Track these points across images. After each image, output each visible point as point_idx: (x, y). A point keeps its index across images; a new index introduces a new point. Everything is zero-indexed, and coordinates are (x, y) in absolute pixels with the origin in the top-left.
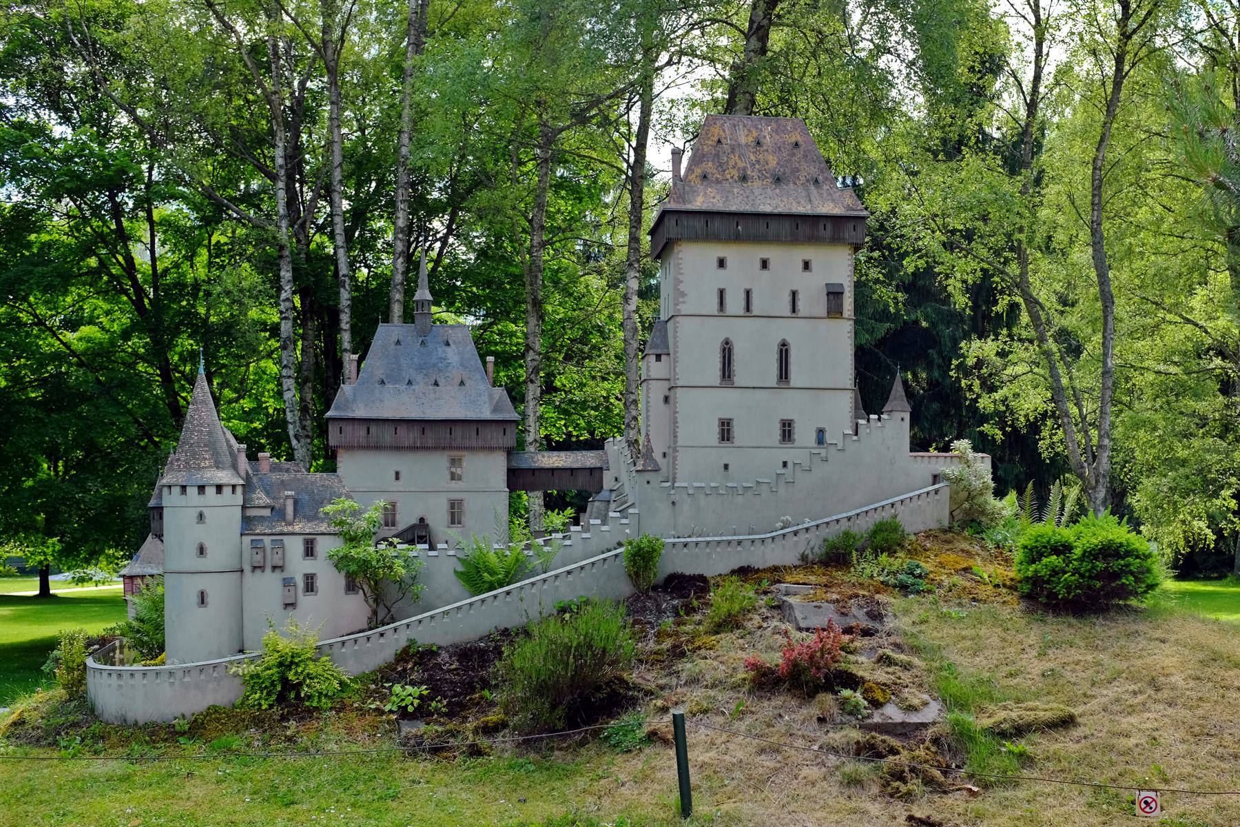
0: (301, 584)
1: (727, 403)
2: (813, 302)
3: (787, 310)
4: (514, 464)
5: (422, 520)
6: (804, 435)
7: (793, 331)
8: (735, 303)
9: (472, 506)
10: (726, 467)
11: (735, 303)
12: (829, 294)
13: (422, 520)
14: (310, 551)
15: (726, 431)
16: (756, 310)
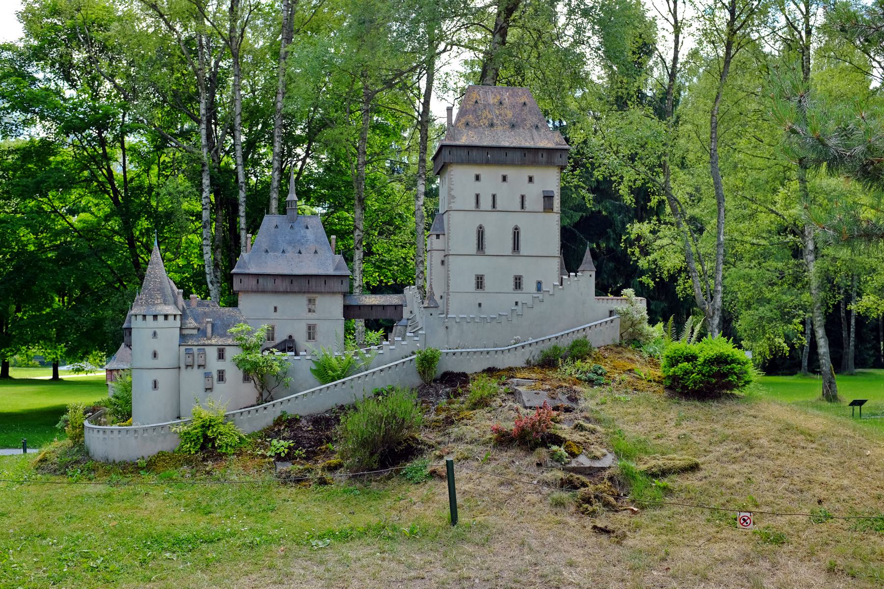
0: (215, 376)
1: (481, 265)
2: (535, 202)
3: (518, 207)
4: (348, 303)
5: (290, 337)
6: (529, 285)
7: (521, 220)
8: (486, 203)
9: (322, 328)
10: (480, 305)
11: (486, 203)
12: (544, 197)
13: (290, 337)
14: (221, 356)
15: (480, 282)
16: (499, 206)
